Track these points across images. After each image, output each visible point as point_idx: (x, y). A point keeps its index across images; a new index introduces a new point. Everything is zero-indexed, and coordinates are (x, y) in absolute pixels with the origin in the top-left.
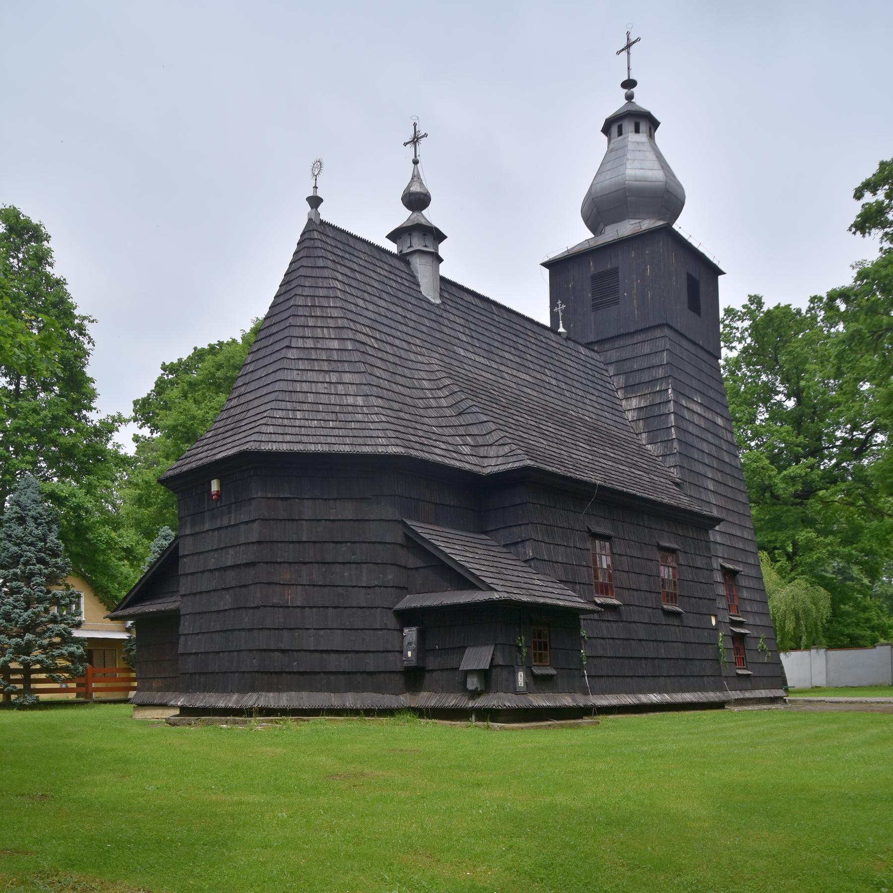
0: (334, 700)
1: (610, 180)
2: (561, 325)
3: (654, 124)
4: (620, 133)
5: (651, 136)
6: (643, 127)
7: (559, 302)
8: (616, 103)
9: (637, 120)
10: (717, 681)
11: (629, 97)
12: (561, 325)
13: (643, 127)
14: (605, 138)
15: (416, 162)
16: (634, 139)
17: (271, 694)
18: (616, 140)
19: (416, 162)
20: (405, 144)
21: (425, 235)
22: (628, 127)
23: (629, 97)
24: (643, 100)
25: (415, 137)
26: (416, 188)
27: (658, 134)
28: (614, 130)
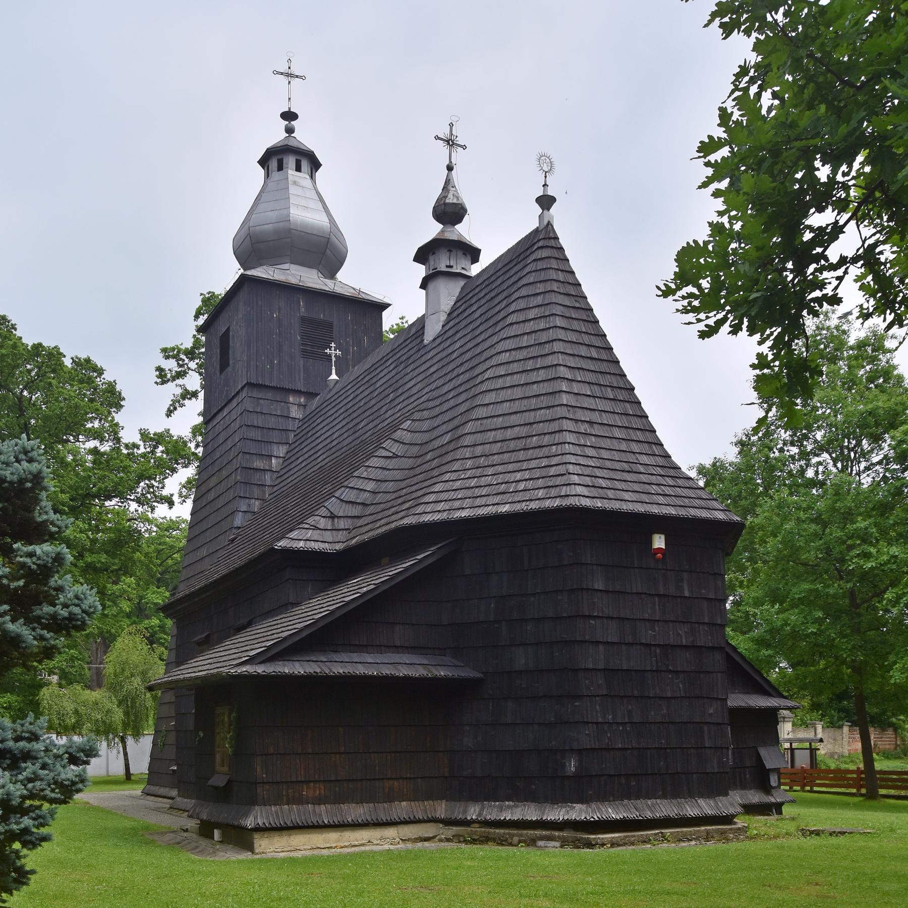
0: (665, 808)
1: (268, 219)
2: (334, 371)
3: (315, 165)
4: (280, 168)
5: (312, 177)
6: (305, 165)
7: (333, 345)
8: (276, 135)
9: (280, 157)
10: (715, 787)
11: (290, 131)
12: (334, 371)
13: (305, 165)
14: (261, 172)
15: (450, 168)
16: (296, 178)
17: (323, 807)
18: (276, 175)
19: (450, 168)
20: (464, 147)
21: (450, 251)
22: (290, 161)
23: (290, 131)
24: (304, 136)
25: (448, 141)
26: (450, 199)
27: (319, 174)
28: (274, 164)
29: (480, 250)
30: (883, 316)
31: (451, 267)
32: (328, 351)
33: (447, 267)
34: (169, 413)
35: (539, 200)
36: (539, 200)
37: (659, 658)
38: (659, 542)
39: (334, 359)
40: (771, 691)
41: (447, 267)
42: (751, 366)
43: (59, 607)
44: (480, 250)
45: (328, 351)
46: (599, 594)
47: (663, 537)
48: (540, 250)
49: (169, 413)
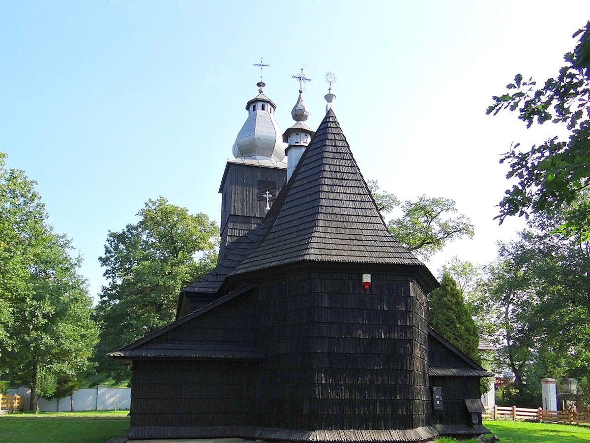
1: (246, 140)
2: (268, 205)
7: (268, 192)
28: (251, 108)
29: (283, 142)
30: (576, 76)
31: (298, 142)
32: (265, 196)
33: (296, 143)
34: (515, 147)
35: (326, 97)
36: (326, 97)
37: (365, 346)
38: (367, 278)
39: (268, 199)
40: (473, 365)
41: (296, 143)
42: (528, 128)
43: (555, 290)
44: (283, 142)
45: (265, 196)
46: (326, 310)
47: (369, 276)
48: (329, 122)
49: (515, 147)
